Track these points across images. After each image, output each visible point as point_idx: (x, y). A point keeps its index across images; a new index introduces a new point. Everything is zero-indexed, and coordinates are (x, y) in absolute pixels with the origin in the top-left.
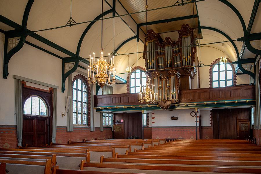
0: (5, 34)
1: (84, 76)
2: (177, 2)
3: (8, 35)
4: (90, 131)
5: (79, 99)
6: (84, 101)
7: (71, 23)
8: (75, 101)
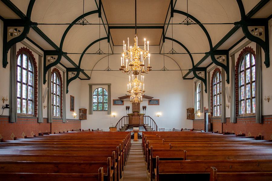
0: (63, 52)
1: (30, 50)
2: (183, 22)
3: (8, 23)
4: (38, 122)
5: (24, 81)
6: (29, 84)
7: (100, 52)
8: (19, 82)
